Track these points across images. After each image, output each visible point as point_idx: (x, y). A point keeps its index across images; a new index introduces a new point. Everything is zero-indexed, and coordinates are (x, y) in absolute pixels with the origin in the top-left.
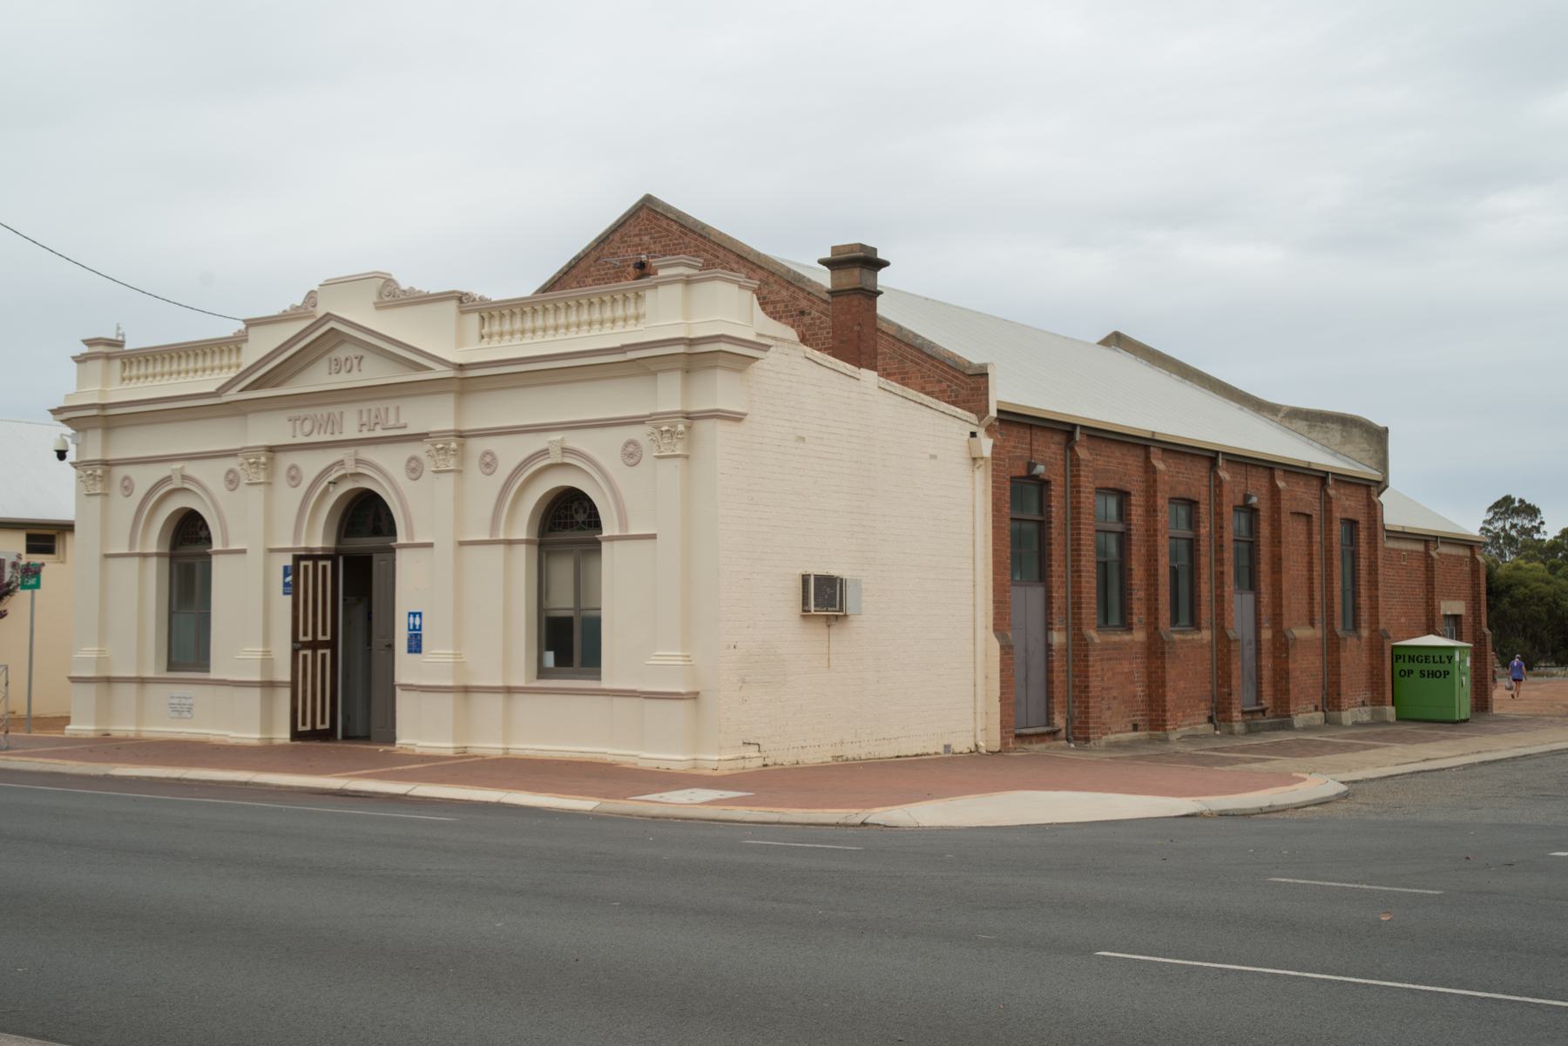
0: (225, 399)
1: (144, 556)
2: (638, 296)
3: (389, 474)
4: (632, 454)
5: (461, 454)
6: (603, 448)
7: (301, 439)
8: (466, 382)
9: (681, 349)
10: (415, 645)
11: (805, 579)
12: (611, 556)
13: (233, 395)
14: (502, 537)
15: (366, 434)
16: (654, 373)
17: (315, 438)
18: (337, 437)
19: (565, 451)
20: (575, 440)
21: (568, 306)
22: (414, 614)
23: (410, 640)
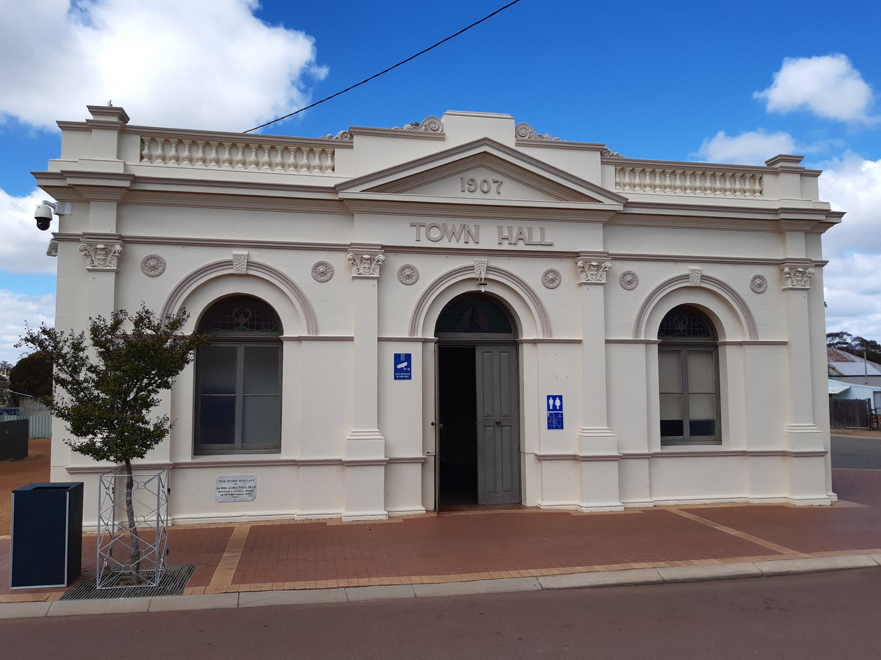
0: (342, 195)
1: (647, 343)
2: (761, 179)
3: (524, 283)
4: (551, 280)
5: (122, 258)
6: (297, 268)
7: (425, 243)
8: (624, 217)
9: (127, 184)
10: (556, 421)
11: (396, 378)
12: (733, 362)
13: (354, 193)
14: (420, 336)
15: (506, 246)
16: (88, 202)
17: (444, 244)
18: (472, 245)
19: (250, 264)
20: (258, 256)
21: (311, 150)
22: (554, 398)
23: (549, 419)
